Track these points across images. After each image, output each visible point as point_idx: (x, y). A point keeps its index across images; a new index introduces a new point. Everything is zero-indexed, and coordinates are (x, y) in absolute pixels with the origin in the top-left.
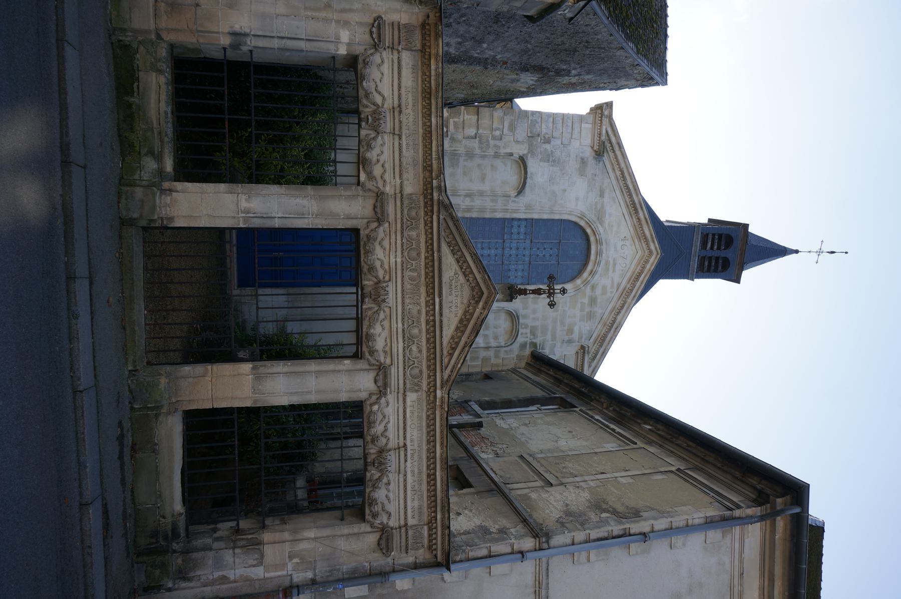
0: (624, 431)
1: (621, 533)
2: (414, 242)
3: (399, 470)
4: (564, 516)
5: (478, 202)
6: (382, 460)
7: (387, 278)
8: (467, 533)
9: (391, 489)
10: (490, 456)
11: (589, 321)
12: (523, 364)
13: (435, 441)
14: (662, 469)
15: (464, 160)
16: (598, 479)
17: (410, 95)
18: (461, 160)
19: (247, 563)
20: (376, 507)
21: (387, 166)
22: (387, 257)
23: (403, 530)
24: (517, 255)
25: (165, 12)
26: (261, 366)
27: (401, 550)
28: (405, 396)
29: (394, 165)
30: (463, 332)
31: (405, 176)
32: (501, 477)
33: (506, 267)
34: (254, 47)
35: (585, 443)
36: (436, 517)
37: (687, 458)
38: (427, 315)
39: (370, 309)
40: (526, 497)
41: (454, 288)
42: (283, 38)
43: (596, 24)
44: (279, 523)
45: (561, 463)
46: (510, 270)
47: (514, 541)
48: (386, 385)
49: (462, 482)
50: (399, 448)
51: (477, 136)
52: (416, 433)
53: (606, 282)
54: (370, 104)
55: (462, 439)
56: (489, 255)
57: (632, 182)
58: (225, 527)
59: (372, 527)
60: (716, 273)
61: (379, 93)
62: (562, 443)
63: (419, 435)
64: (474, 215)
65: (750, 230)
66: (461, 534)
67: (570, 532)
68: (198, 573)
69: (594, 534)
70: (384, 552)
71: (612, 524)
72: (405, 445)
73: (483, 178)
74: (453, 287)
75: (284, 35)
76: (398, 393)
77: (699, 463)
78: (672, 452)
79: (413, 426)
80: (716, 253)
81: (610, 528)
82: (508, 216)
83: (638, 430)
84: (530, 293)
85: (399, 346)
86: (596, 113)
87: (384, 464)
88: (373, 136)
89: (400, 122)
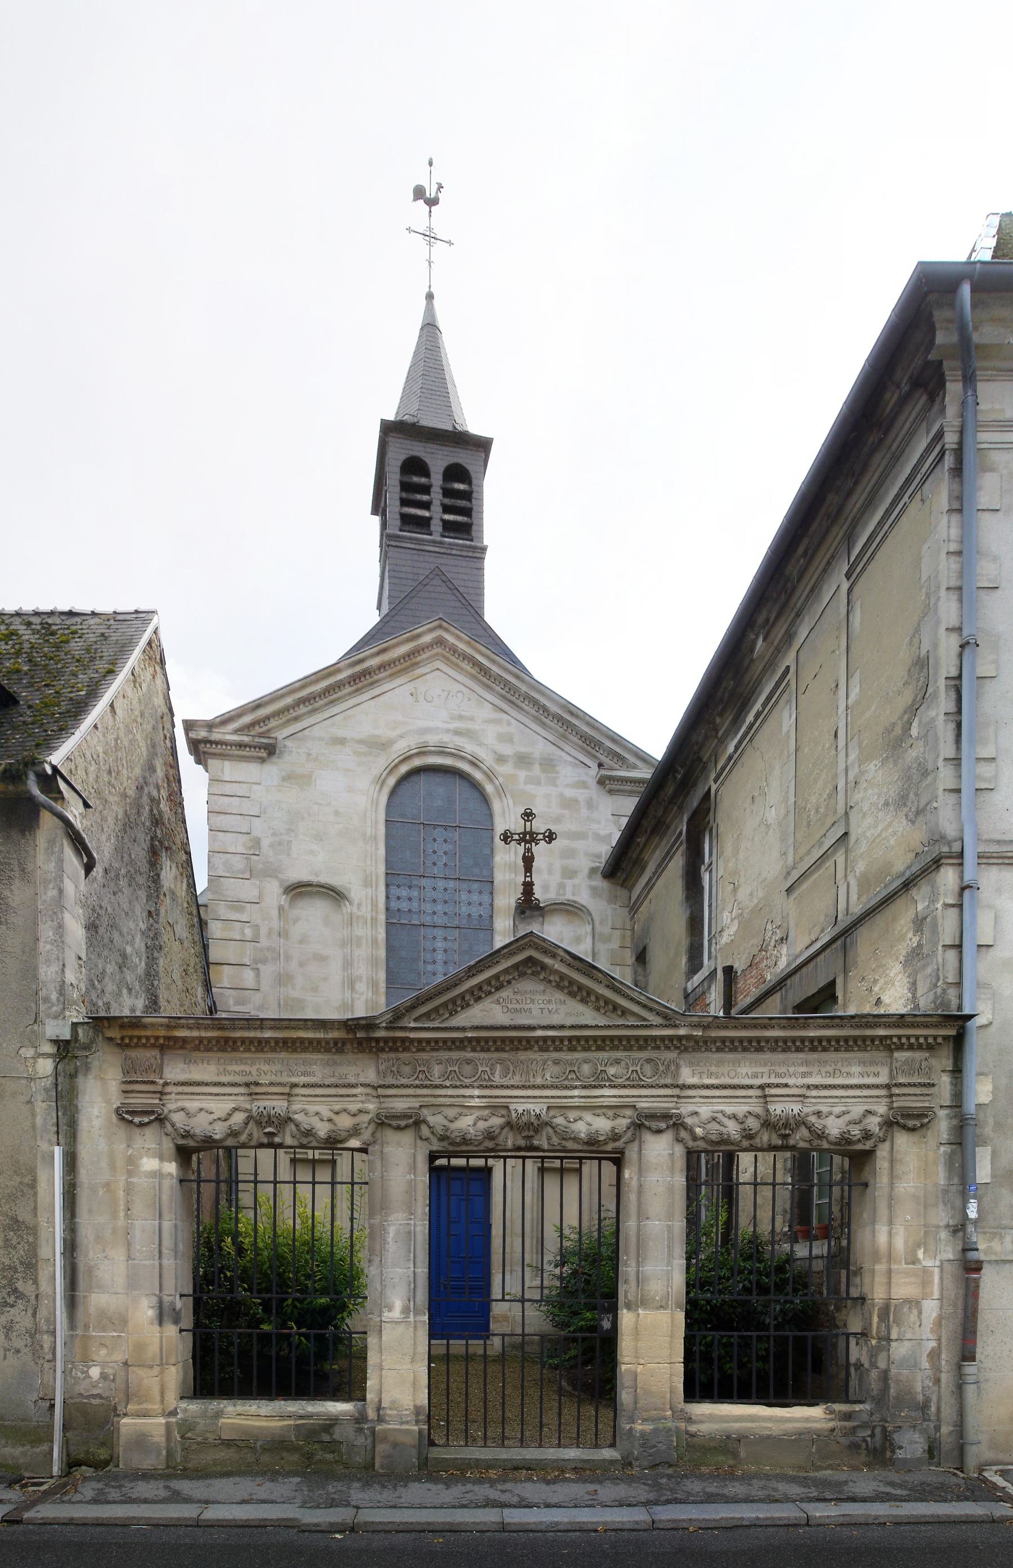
0: (760, 694)
1: (953, 695)
2: (450, 1069)
3: (800, 1096)
4: (906, 809)
5: (362, 970)
6: (781, 1122)
7: (504, 1112)
8: (913, 987)
9: (829, 1109)
10: (784, 951)
11: (558, 768)
12: (622, 893)
13: (759, 1040)
14: (843, 610)
15: (294, 989)
16: (847, 744)
17: (230, 1068)
18: (294, 994)
19: (915, 1323)
20: (853, 1133)
21: (337, 1107)
22: (473, 1111)
23: (896, 1091)
24: (446, 902)
25: (139, 1404)
26: (626, 1297)
27: (928, 1095)
28: (684, 1087)
29: (336, 1096)
30: (589, 992)
31: (352, 1080)
32: (822, 931)
33: (464, 921)
34: (176, 1290)
35: (777, 772)
36: (882, 1038)
37: (828, 556)
38: (561, 1050)
39: (549, 1139)
40: (864, 883)
41: (521, 1006)
42: (160, 1252)
43: (93, 763)
44: (858, 1279)
45: (809, 816)
46: (469, 915)
47: (941, 902)
48: (666, 1116)
49: (827, 995)
50: (765, 1096)
51: (255, 966)
52: (744, 1070)
53: (490, 735)
54: (247, 1131)
55: (749, 1000)
56: (445, 951)
57: (317, 681)
58: (856, 1353)
59: (884, 1140)
60: (474, 495)
61: (230, 1115)
62: (772, 815)
63: (747, 1064)
64: (382, 976)
65: (391, 417)
66: (914, 997)
67: (936, 797)
68: (919, 1389)
69: (948, 750)
70: (926, 1120)
71: (934, 714)
72: (762, 1087)
73: (321, 959)
74: (518, 1006)
75: (157, 1250)
76: (679, 1097)
77: (841, 528)
78: (812, 591)
79: (732, 1074)
80: (436, 496)
81: (942, 717)
82: (382, 917)
83: (763, 664)
84: (531, 876)
85: (608, 1095)
86: (204, 753)
87: (787, 1120)
88: (293, 1127)
89: (271, 1084)
